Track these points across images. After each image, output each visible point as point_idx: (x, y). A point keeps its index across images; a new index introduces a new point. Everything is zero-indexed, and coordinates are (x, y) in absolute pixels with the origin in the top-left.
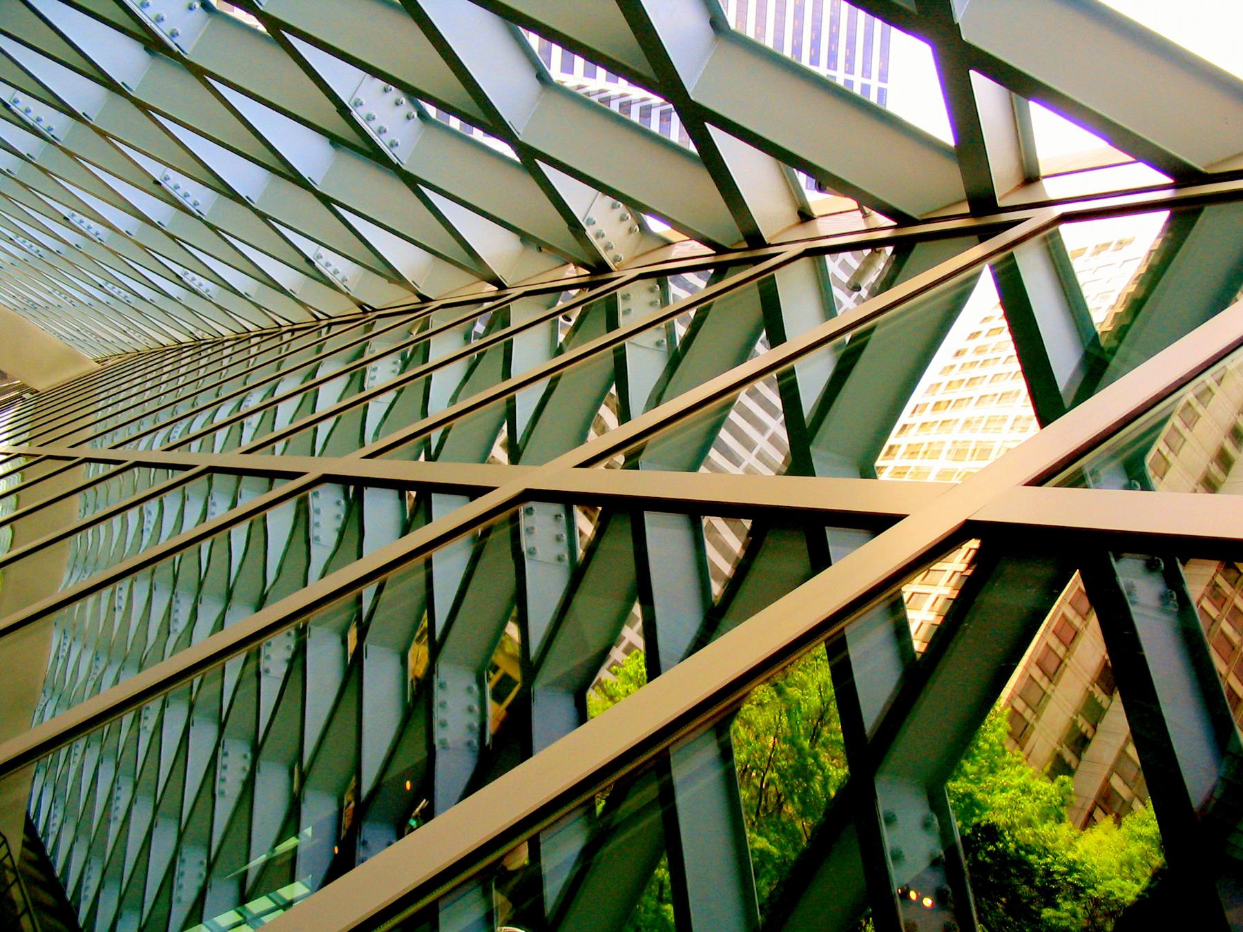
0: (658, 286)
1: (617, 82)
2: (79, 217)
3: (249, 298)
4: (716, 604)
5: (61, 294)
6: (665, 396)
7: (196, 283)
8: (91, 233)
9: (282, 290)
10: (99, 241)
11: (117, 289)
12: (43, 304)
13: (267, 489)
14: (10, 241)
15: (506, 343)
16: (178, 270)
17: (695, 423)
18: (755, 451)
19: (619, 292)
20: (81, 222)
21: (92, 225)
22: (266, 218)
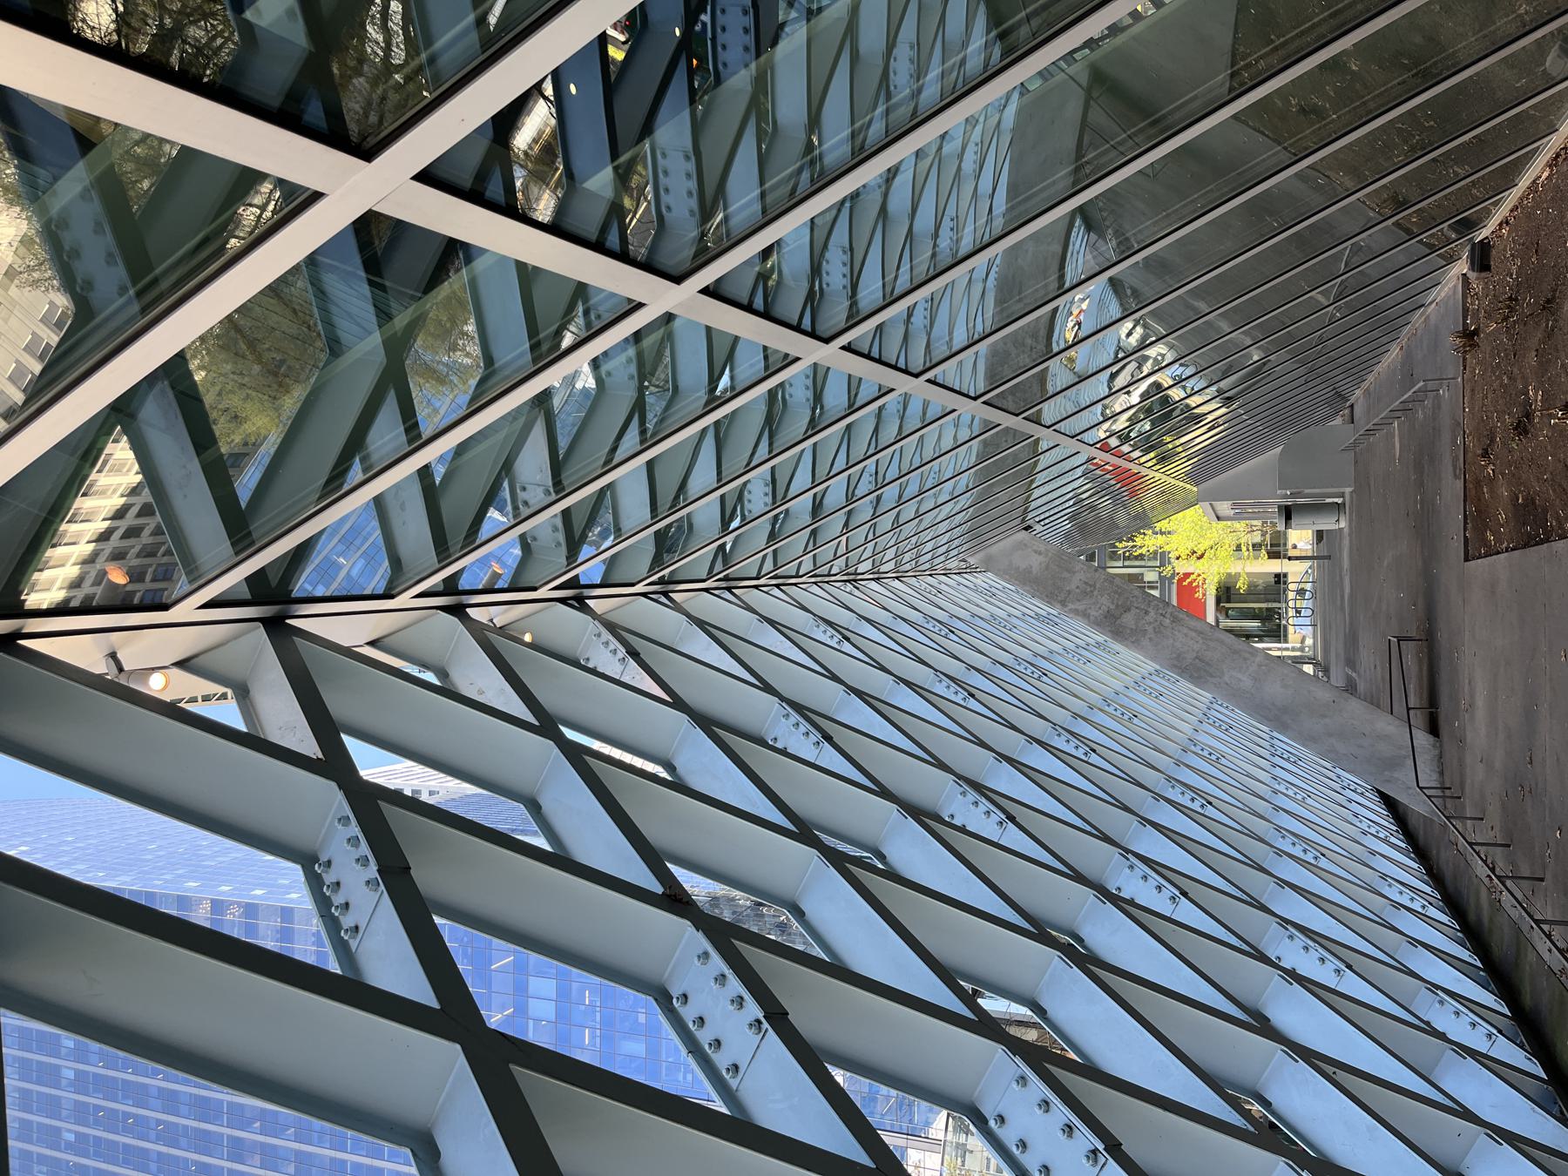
0: (529, 541)
1: (413, 791)
2: (1080, 753)
3: (757, 617)
4: (313, 50)
5: (1073, 657)
6: (659, 341)
7: (829, 634)
8: (1179, 788)
9: (860, 694)
10: (1057, 727)
11: (1028, 672)
12: (1090, 648)
13: (693, 514)
14: (1136, 714)
15: (657, 516)
16: (972, 704)
17: (674, 422)
18: (200, 699)
19: (554, 497)
20: (1193, 800)
21: (829, 639)
22: (882, 792)
